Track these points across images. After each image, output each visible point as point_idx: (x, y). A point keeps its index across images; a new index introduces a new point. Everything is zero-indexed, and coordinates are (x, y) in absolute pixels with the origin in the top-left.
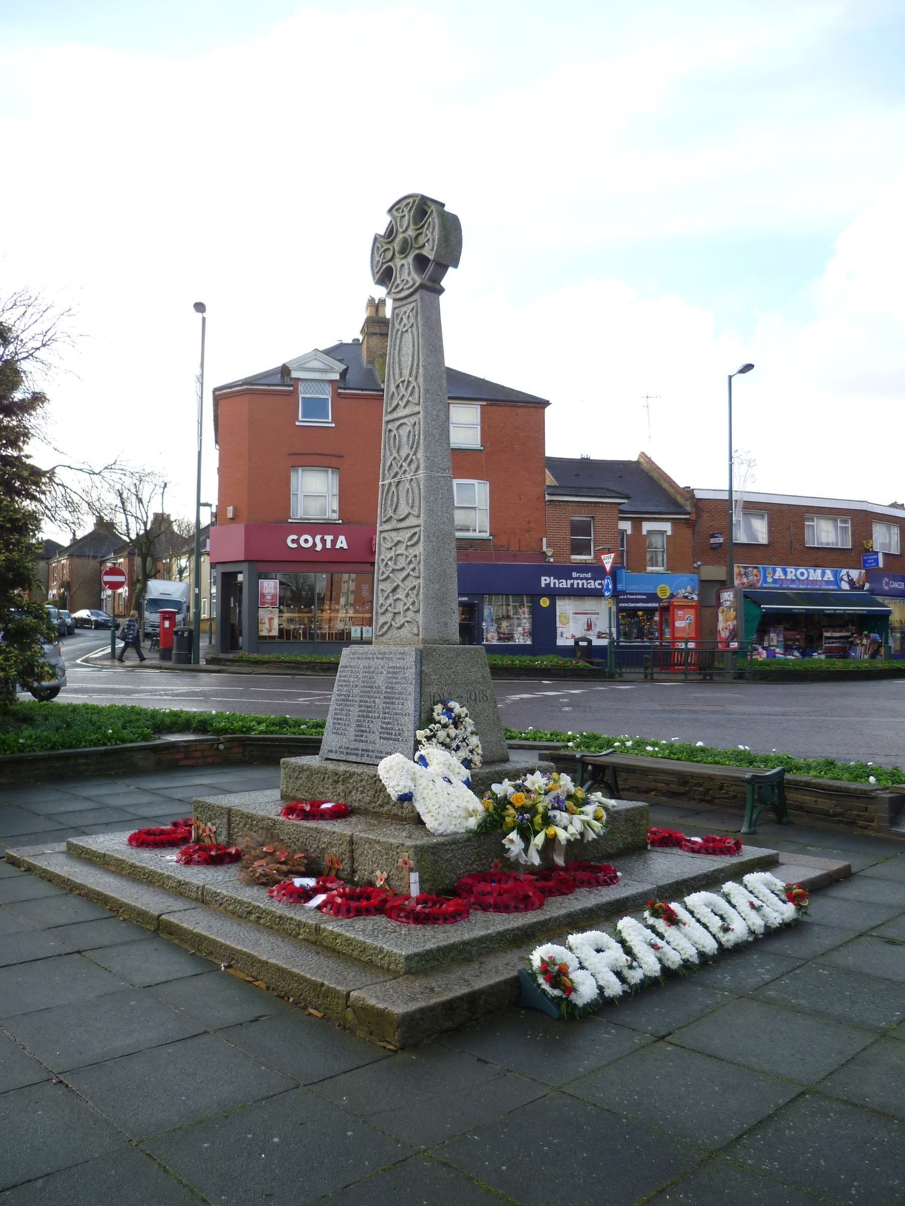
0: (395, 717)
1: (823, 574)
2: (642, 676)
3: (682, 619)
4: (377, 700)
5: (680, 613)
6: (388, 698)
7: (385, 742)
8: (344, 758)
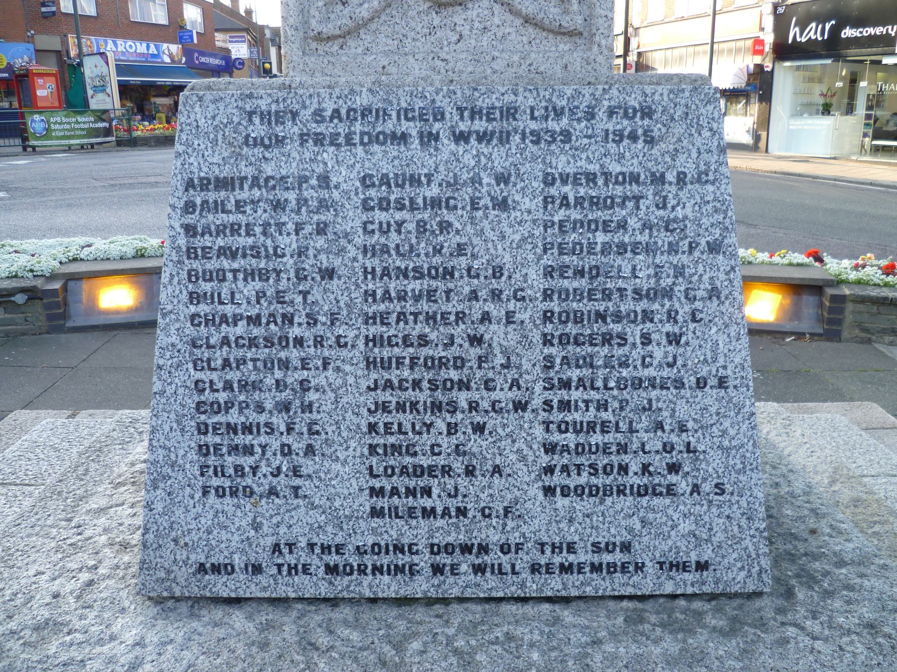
0: (638, 398)
1: (148, 47)
2: (20, 149)
3: (43, 87)
4: (495, 333)
5: (40, 81)
6: (566, 317)
7: (586, 504)
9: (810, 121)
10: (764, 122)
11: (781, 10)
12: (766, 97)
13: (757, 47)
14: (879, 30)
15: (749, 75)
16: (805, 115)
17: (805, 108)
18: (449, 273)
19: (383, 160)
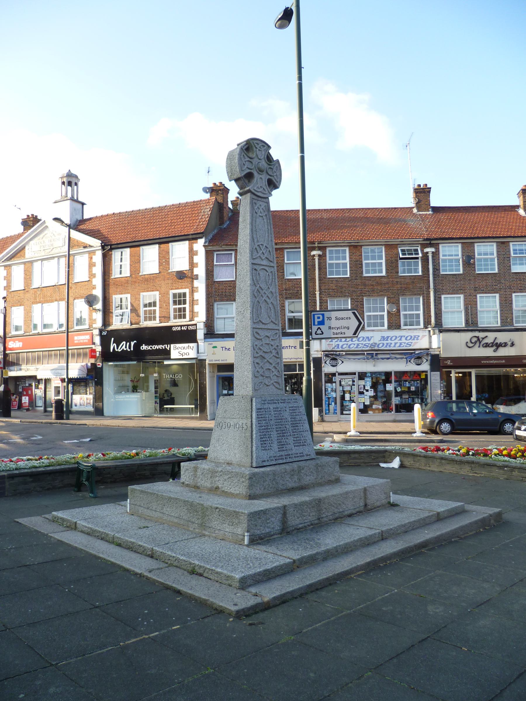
0: (300, 433)
4: (287, 426)
7: (298, 448)
8: (275, 463)
9: (128, 396)
10: (99, 397)
11: (104, 333)
12: (99, 383)
13: (93, 354)
14: (160, 347)
15: (88, 369)
16: (123, 393)
17: (121, 389)
18: (282, 419)
19: (275, 406)
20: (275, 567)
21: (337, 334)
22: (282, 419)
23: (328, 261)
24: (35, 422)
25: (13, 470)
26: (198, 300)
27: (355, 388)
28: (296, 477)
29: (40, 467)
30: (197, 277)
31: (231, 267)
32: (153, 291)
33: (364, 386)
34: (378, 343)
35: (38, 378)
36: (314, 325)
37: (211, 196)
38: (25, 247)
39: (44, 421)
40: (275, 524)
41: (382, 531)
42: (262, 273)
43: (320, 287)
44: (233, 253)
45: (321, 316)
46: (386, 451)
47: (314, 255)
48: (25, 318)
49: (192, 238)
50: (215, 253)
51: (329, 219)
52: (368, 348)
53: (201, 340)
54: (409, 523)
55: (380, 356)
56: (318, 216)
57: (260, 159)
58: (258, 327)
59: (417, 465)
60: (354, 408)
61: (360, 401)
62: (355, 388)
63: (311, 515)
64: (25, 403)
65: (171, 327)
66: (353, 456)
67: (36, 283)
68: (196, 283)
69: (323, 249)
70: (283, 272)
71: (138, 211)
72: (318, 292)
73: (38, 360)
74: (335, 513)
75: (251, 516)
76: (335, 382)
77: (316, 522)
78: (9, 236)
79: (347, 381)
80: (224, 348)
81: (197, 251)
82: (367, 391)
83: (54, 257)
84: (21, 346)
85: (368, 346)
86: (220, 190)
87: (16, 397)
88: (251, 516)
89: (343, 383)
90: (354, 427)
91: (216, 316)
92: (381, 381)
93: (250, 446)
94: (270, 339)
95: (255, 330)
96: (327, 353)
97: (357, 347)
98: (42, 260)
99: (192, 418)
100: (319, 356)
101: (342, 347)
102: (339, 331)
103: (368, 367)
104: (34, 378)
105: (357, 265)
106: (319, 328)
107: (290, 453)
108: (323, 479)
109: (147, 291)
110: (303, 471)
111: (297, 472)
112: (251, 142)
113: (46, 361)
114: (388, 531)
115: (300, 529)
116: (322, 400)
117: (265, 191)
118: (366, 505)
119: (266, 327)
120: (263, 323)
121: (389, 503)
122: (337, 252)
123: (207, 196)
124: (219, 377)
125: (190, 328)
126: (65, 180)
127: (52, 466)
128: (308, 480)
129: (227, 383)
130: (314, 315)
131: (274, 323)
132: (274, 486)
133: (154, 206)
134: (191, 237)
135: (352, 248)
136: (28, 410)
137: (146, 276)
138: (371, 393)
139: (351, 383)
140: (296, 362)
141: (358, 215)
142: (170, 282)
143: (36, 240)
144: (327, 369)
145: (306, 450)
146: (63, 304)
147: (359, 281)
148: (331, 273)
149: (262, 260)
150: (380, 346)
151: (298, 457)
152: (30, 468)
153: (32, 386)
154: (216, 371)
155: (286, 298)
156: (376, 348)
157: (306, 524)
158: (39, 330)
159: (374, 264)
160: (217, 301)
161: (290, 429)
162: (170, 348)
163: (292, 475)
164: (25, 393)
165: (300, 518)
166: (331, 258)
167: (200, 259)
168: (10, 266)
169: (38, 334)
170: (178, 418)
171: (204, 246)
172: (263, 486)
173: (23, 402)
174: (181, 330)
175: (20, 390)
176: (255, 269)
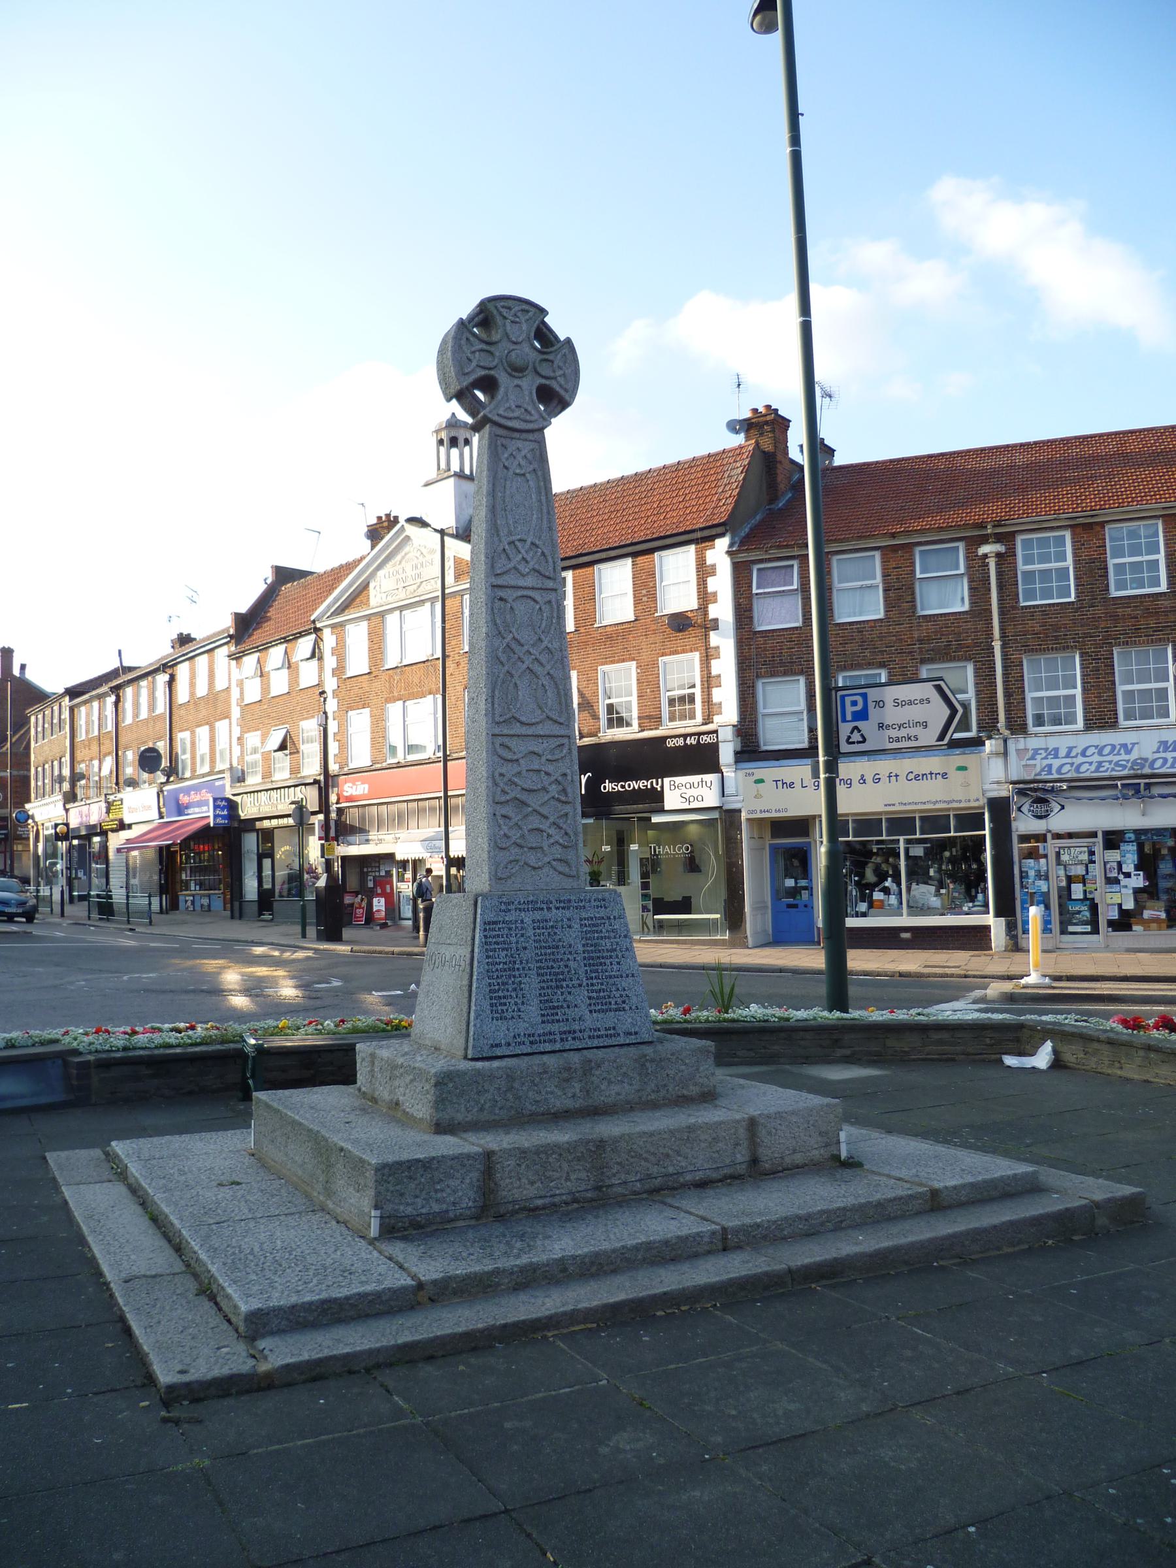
0: (611, 981)
4: (571, 963)
7: (601, 1015)
8: (529, 1050)
14: (642, 784)
19: (538, 915)
20: (359, 1294)
21: (898, 740)
22: (557, 947)
23: (1021, 567)
24: (380, 952)
25: (118, 1050)
26: (719, 676)
27: (1096, 870)
28: (577, 1086)
29: (178, 1046)
30: (715, 625)
31: (791, 598)
32: (623, 661)
33: (1120, 865)
34: (1151, 757)
35: (399, 857)
36: (844, 720)
37: (747, 438)
38: (367, 585)
39: (397, 949)
40: (461, 1193)
41: (724, 1229)
42: (521, 608)
43: (1002, 629)
44: (795, 563)
45: (860, 699)
46: (1021, 1026)
47: (985, 556)
48: (373, 732)
49: (703, 537)
50: (755, 568)
51: (1027, 467)
52: (1125, 772)
53: (728, 765)
54: (822, 1212)
55: (1156, 791)
56: (1004, 460)
57: (515, 343)
58: (505, 732)
59: (1092, 1063)
60: (1035, 916)
61: (1109, 901)
62: (1096, 870)
63: (573, 1177)
64: (378, 911)
65: (663, 739)
66: (936, 1036)
67: (392, 661)
68: (714, 639)
69: (1007, 538)
70: (913, 601)
71: (591, 487)
72: (999, 643)
73: (400, 820)
74: (649, 1177)
75: (386, 1171)
76: (1045, 856)
77: (589, 1195)
78: (344, 563)
79: (1076, 853)
80: (780, 784)
81: (714, 566)
82: (1128, 875)
83: (423, 602)
84: (366, 792)
85: (1124, 767)
86: (766, 423)
87: (362, 900)
88: (386, 1171)
89: (1065, 858)
90: (1036, 966)
91: (761, 710)
92: (1164, 851)
93: (465, 1009)
94: (544, 758)
95: (499, 740)
96: (1021, 786)
97: (1097, 770)
98: (401, 608)
99: (715, 943)
100: (1004, 794)
101: (1059, 771)
102: (903, 732)
103: (1128, 817)
104: (391, 856)
105: (1092, 571)
106: (856, 728)
107: (577, 1028)
108: (663, 1093)
109: (613, 662)
110: (597, 1073)
111: (580, 1073)
112: (490, 306)
113: (413, 823)
114: (743, 1230)
115: (537, 1208)
116: (1014, 899)
117: (531, 415)
118: (754, 1161)
119: (530, 731)
120: (522, 723)
121: (836, 1158)
122: (1044, 543)
123: (739, 439)
124: (774, 849)
125: (705, 739)
126: (443, 435)
127: (207, 1044)
128: (610, 1093)
129: (796, 863)
130: (843, 697)
131: (556, 722)
132: (509, 1104)
133: (626, 474)
134: (699, 535)
135: (1078, 530)
136: (384, 926)
137: (608, 629)
138: (1138, 881)
139: (1085, 857)
140: (949, 809)
141: (1102, 450)
142: (659, 638)
143: (388, 568)
144: (1024, 823)
145: (626, 1021)
146: (439, 698)
147: (1099, 611)
148: (1030, 595)
149: (524, 576)
150: (1158, 764)
151: (598, 1037)
152: (156, 1047)
153: (392, 876)
154: (768, 834)
155: (923, 661)
156: (1147, 771)
157: (557, 1200)
158: (400, 757)
159: (1137, 567)
160: (763, 677)
161: (581, 972)
162: (662, 787)
163: (567, 1080)
164: (379, 891)
165: (539, 1184)
166: (1028, 560)
167: (722, 583)
168: (342, 625)
169: (399, 766)
170: (684, 942)
171: (728, 552)
172: (477, 1102)
173: (375, 909)
174: (686, 744)
175: (371, 884)
176: (501, 599)
